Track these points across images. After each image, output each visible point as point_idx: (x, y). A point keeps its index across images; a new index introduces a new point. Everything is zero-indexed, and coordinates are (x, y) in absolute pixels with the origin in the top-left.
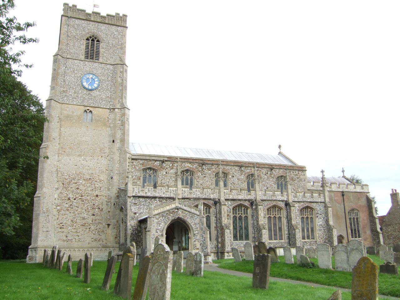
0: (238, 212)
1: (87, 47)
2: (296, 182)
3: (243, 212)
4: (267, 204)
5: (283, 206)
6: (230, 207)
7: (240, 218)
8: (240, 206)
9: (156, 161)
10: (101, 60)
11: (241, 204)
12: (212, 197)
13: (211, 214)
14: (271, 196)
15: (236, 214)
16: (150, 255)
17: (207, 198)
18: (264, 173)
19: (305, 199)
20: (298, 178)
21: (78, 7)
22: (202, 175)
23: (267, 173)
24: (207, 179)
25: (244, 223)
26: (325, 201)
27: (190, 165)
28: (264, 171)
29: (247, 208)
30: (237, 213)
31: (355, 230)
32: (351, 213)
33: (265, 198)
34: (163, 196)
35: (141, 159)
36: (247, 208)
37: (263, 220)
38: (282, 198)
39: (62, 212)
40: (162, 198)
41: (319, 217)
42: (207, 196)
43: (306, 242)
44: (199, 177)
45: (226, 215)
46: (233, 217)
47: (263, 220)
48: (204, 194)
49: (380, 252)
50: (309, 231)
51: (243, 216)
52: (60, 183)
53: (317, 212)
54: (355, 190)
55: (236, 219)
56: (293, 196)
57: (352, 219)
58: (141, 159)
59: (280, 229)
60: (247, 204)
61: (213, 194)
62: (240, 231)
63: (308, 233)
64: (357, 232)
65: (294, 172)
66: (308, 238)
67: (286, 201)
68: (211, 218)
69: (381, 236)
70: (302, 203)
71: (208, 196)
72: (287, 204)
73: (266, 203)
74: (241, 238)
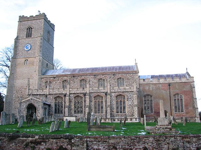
0: (77, 100)
1: (27, 32)
2: (130, 80)
9: (51, 78)
10: (32, 36)
15: (118, 100)
16: (172, 124)
19: (119, 91)
20: (132, 78)
21: (25, 16)
23: (111, 77)
24: (75, 84)
27: (66, 78)
31: (179, 107)
34: (41, 94)
35: (45, 78)
39: (16, 102)
40: (41, 95)
43: (118, 115)
52: (15, 91)
54: (180, 81)
58: (45, 78)
59: (102, 108)
60: (82, 95)
66: (121, 112)
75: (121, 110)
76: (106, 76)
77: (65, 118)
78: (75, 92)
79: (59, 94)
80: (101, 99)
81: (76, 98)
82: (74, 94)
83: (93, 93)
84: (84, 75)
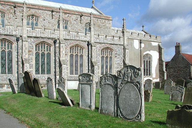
0: (40, 49)
3: (46, 49)
4: (70, 43)
5: (85, 46)
6: (32, 44)
7: (43, 55)
8: (43, 43)
11: (44, 41)
12: (14, 33)
13: (13, 50)
14: (75, 36)
17: (9, 34)
18: (74, 19)
19: (106, 41)
22: (13, 16)
25: (47, 59)
26: (124, 44)
28: (74, 17)
29: (50, 45)
30: (40, 50)
31: (147, 70)
32: (146, 57)
33: (68, 38)
36: (50, 45)
37: (65, 57)
38: (85, 39)
41: (117, 57)
42: (9, 32)
44: (10, 19)
45: (27, 51)
46: (36, 53)
47: (65, 57)
48: (6, 30)
49: (165, 87)
50: (108, 69)
51: (46, 53)
53: (116, 53)
55: (39, 55)
56: (96, 38)
57: (146, 61)
61: (15, 31)
62: (42, 65)
63: (106, 70)
64: (148, 71)
65: (101, 21)
67: (88, 42)
68: (13, 53)
69: (165, 74)
70: (103, 45)
71: (10, 32)
72: (89, 44)
73: (69, 42)
74: (43, 72)
75: (106, 70)
76: (69, 15)
77: (155, 81)
78: (38, 36)
79: (5, 35)
80: (80, 51)
81: (39, 47)
82: (35, 37)
83: (68, 40)
84: (34, 7)
